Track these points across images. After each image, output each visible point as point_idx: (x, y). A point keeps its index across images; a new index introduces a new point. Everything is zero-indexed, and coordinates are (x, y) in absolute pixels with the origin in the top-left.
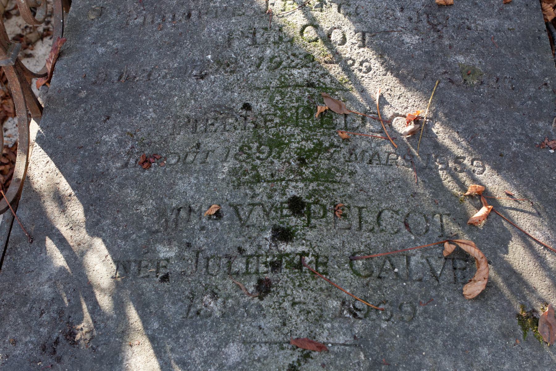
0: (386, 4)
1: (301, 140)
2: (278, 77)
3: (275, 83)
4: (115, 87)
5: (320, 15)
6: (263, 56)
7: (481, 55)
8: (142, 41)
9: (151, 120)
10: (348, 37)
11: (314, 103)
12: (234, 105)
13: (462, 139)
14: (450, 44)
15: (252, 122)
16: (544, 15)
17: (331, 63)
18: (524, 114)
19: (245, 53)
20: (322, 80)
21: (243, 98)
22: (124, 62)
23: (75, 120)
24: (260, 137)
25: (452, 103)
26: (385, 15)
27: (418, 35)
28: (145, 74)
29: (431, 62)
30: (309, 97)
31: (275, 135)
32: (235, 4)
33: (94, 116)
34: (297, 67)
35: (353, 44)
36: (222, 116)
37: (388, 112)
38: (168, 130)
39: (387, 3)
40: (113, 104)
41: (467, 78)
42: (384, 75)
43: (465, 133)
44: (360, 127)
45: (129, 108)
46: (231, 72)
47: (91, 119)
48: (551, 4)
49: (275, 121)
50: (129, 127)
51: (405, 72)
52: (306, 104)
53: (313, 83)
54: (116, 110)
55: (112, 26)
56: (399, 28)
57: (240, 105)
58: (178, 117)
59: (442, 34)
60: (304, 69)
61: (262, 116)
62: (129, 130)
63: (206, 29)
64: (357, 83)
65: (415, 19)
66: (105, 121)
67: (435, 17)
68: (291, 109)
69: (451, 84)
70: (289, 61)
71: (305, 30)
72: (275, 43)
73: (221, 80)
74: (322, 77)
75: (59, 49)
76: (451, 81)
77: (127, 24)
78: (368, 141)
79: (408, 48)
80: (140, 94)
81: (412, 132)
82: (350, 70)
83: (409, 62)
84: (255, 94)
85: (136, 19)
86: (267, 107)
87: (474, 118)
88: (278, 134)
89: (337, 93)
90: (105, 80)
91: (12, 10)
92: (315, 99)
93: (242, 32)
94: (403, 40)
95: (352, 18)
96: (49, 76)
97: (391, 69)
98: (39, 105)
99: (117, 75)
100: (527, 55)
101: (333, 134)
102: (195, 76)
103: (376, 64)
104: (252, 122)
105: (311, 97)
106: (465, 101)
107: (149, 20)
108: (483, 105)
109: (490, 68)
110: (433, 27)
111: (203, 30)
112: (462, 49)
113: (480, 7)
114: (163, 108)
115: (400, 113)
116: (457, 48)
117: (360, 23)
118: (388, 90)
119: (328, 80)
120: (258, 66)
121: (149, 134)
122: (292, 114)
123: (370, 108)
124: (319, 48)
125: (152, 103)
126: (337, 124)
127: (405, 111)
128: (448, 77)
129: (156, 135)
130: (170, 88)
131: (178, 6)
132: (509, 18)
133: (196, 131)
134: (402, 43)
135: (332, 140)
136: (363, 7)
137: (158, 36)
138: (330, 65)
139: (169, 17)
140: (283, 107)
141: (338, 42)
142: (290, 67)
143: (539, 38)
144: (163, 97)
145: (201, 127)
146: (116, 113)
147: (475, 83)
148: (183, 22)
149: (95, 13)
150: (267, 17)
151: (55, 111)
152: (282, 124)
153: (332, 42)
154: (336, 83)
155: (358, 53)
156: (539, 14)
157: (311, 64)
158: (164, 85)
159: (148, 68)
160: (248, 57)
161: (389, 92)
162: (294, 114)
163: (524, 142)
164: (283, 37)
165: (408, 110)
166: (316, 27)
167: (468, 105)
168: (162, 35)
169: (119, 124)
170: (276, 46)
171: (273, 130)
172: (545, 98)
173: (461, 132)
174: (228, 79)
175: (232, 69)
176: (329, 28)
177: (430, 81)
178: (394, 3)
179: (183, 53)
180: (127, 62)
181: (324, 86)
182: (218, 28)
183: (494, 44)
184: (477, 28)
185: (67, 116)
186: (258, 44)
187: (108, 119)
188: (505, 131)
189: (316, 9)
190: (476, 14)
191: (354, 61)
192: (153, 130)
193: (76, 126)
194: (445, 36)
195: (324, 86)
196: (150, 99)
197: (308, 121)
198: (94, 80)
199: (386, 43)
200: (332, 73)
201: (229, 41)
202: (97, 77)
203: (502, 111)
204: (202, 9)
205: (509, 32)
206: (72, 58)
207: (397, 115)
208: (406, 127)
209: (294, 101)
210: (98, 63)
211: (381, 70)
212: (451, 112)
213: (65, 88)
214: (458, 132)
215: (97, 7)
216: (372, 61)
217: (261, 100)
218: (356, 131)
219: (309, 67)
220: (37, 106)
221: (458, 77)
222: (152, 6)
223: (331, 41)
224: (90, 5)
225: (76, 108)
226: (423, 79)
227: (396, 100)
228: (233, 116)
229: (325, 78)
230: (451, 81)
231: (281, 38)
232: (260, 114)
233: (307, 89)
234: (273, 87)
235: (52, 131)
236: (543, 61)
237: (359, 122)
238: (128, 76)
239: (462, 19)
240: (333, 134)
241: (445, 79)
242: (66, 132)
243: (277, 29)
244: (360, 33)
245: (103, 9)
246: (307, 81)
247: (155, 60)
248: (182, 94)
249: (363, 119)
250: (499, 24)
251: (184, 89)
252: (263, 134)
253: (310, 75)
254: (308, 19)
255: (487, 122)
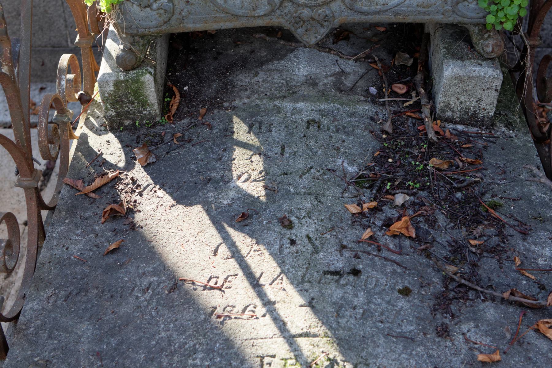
0: (414, 363)
39: (416, 360)
131: (147, 362)
178: (425, 361)
215: (40, 359)
222: (113, 361)
224: (32, 356)
245: (48, 363)
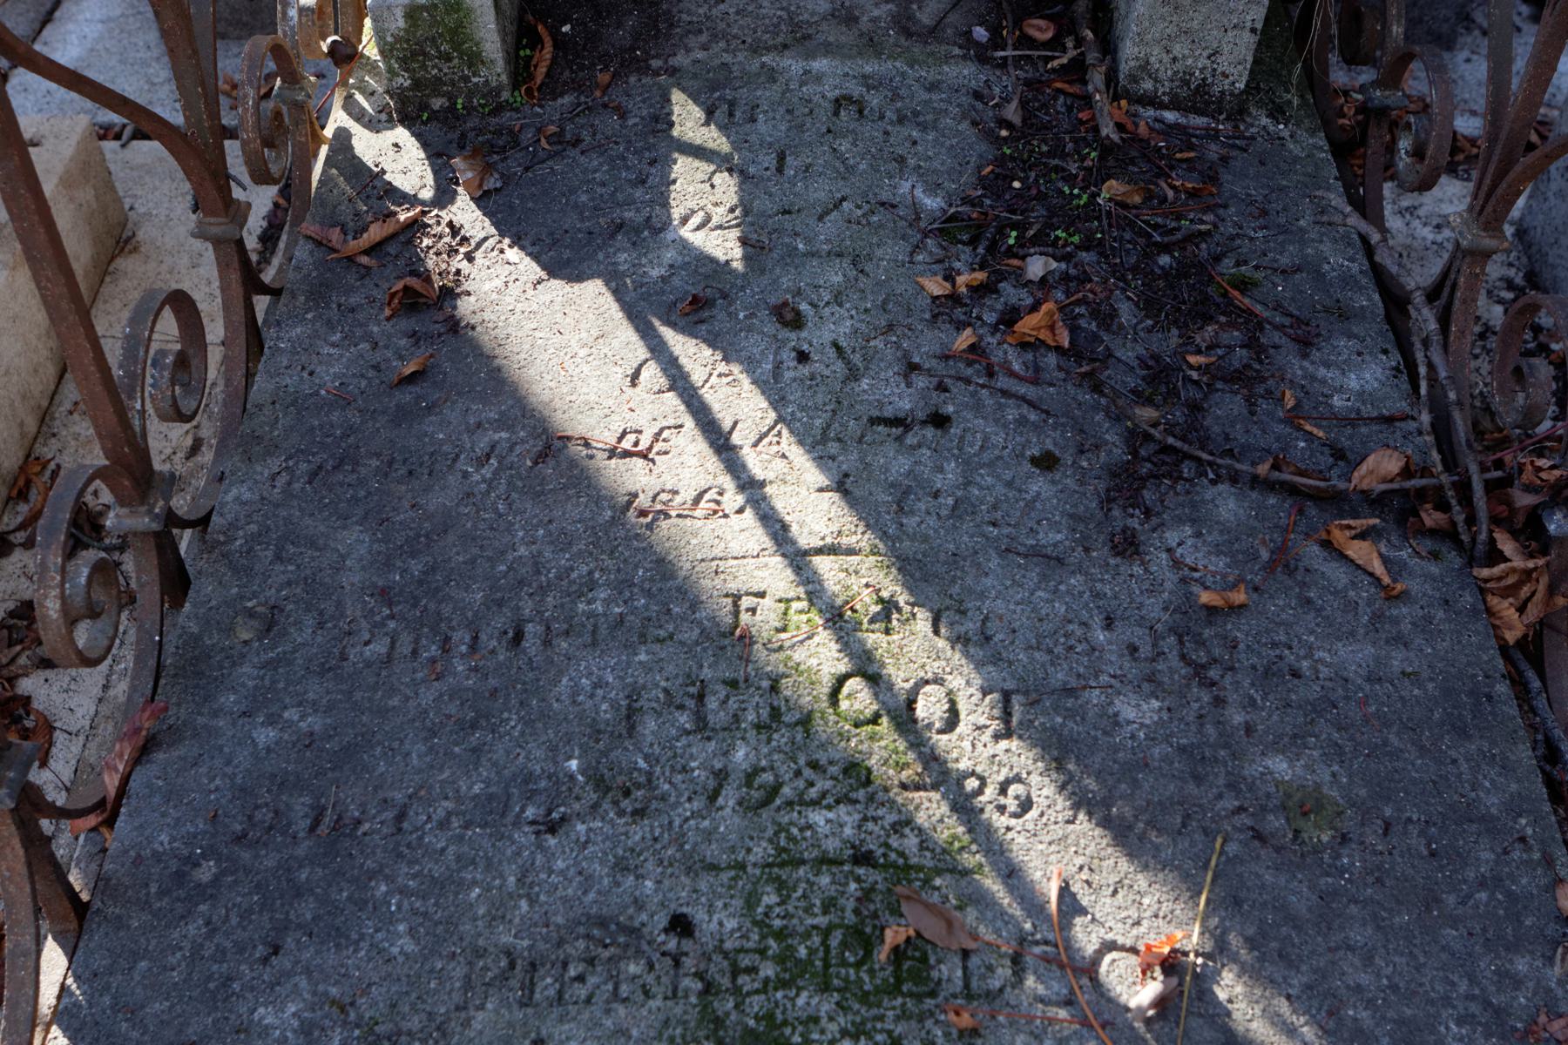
1: (838, 1036)
2: (770, 832)
3: (761, 851)
4: (300, 851)
5: (884, 645)
6: (725, 767)
7: (1335, 753)
8: (383, 712)
9: (401, 959)
10: (963, 707)
11: (875, 915)
12: (644, 917)
13: (1302, 1020)
14: (1247, 723)
15: (696, 974)
16: (1495, 627)
17: (918, 788)
18: (1470, 934)
19: (675, 756)
20: (894, 842)
21: (671, 895)
22: (330, 775)
23: (178, 955)
24: (719, 1022)
25: (1265, 903)
26: (1062, 640)
27: (1157, 698)
28: (389, 815)
29: (1198, 779)
30: (858, 899)
31: (763, 1018)
32: (646, 607)
33: (235, 943)
34: (824, 802)
35: (978, 728)
36: (606, 954)
37: (1086, 938)
38: (450, 993)
40: (291, 905)
41: (1301, 823)
42: (1068, 822)
43: (1309, 998)
44: (1008, 989)
45: (339, 921)
46: (635, 813)
47: (224, 952)
48: (1511, 600)
49: (762, 974)
50: (336, 983)
51: (1128, 812)
52: (850, 918)
53: (871, 852)
54: (299, 926)
55: (300, 662)
56: (1104, 678)
57: (662, 920)
58: (480, 953)
59: (1222, 694)
60: (842, 808)
61: (726, 955)
62: (334, 991)
63: (565, 680)
64: (995, 850)
65: (1145, 650)
66: (265, 960)
67: (1201, 643)
68: (807, 935)
69: (1257, 843)
70: (801, 784)
71: (845, 690)
72: (758, 727)
73: (607, 838)
74: (896, 832)
75: (144, 733)
76: (1259, 836)
77: (344, 657)
78: (1032, 1033)
79: (1133, 737)
80: (372, 875)
81: (1161, 1003)
82: (972, 810)
83: (1135, 781)
84: (703, 886)
85: (367, 643)
86: (740, 929)
87: (1330, 950)
88: (770, 1016)
89: (938, 882)
90: (271, 828)
91: (13, 531)
92: (878, 903)
93: (666, 691)
94: (1116, 715)
95: (972, 650)
96: (109, 806)
97: (1089, 804)
98: (73, 896)
99: (306, 816)
100: (1462, 750)
101: (932, 1014)
102: (533, 823)
103: (1043, 789)
104: (696, 974)
105: (867, 895)
106: (1301, 900)
107: (405, 648)
108: (1353, 909)
109: (1363, 792)
110: (1197, 674)
111: (556, 682)
112: (1281, 737)
113: (1319, 610)
114: (437, 923)
115: (1120, 940)
116: (1266, 732)
117: (995, 664)
118: (1081, 868)
119: (911, 842)
120: (713, 797)
121: (393, 1006)
122: (812, 952)
123: (1034, 926)
124: (883, 743)
125: (406, 904)
126: (940, 980)
127: (1135, 932)
128: (1249, 822)
129: (413, 1006)
130: (459, 858)
131: (489, 609)
132: (1400, 640)
133: (531, 998)
134: (1116, 722)
135: (928, 1033)
136: (1001, 618)
137: (427, 696)
138: (917, 795)
139: (461, 638)
140: (786, 927)
141: (937, 725)
142: (802, 802)
143: (1489, 698)
144: (438, 886)
145: (546, 988)
146: (298, 934)
147: (1325, 838)
148: (501, 658)
149: (255, 623)
150: (738, 649)
151: (120, 923)
152: (783, 984)
153: (920, 724)
154: (933, 851)
155: (994, 756)
156: (1480, 626)
157: (861, 794)
158: (443, 850)
159: (399, 796)
160: (684, 770)
161: (1084, 875)
162: (817, 950)
163: (1480, 1023)
164: (783, 709)
165: (1142, 929)
166: (874, 679)
167: (1310, 909)
168: (441, 695)
169: (308, 971)
170: (763, 737)
171: (756, 1003)
172: (1524, 881)
173: (1299, 997)
174: (626, 834)
175: (638, 806)
176: (912, 682)
177: (1199, 837)
179: (499, 754)
180: (337, 774)
181: (901, 861)
182: (600, 679)
183: (1366, 720)
184: (1317, 671)
185: (154, 942)
186: (713, 730)
187: (276, 953)
188: (1421, 990)
189: (873, 627)
190: (1312, 632)
191: (983, 781)
192: (407, 993)
193: (180, 973)
194: (1233, 697)
195: (901, 861)
196: (401, 893)
197: (857, 973)
198: (239, 828)
199: (1071, 724)
200: (921, 819)
201: (631, 716)
202: (250, 818)
203: (1408, 924)
204: (556, 619)
205: (1407, 682)
206: (179, 757)
207: (1110, 946)
208: (1138, 988)
209: (816, 910)
210: (255, 775)
211: (1059, 808)
212: (1262, 933)
213: (155, 853)
214: (1288, 997)
215: (259, 604)
216: (1035, 779)
217: (720, 904)
218: (998, 1001)
219: (856, 801)
220: (67, 904)
221: (1275, 822)
222: (415, 606)
223: (915, 721)
225: (183, 917)
226: (1180, 833)
227: (1108, 901)
228: (639, 952)
229: (903, 836)
230: (1259, 836)
231: (775, 713)
232: (719, 949)
233: (852, 872)
234: (755, 865)
235: (107, 987)
236: (1507, 769)
237: (1004, 972)
238: (340, 818)
239: (1275, 645)
240: (932, 1014)
241: (1240, 830)
242: (149, 993)
243: (765, 684)
244: (995, 696)
246: (853, 847)
247: (420, 771)
248: (494, 878)
249: (1016, 960)
250: (1377, 659)
251: (500, 862)
252: (727, 1014)
253: (860, 827)
254: (851, 656)
255: (1368, 960)
